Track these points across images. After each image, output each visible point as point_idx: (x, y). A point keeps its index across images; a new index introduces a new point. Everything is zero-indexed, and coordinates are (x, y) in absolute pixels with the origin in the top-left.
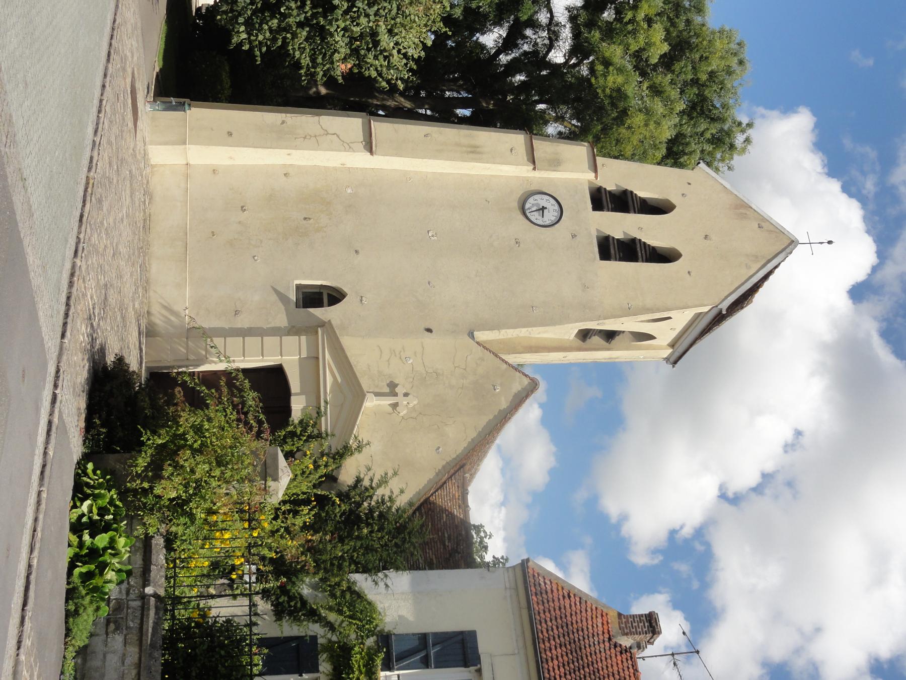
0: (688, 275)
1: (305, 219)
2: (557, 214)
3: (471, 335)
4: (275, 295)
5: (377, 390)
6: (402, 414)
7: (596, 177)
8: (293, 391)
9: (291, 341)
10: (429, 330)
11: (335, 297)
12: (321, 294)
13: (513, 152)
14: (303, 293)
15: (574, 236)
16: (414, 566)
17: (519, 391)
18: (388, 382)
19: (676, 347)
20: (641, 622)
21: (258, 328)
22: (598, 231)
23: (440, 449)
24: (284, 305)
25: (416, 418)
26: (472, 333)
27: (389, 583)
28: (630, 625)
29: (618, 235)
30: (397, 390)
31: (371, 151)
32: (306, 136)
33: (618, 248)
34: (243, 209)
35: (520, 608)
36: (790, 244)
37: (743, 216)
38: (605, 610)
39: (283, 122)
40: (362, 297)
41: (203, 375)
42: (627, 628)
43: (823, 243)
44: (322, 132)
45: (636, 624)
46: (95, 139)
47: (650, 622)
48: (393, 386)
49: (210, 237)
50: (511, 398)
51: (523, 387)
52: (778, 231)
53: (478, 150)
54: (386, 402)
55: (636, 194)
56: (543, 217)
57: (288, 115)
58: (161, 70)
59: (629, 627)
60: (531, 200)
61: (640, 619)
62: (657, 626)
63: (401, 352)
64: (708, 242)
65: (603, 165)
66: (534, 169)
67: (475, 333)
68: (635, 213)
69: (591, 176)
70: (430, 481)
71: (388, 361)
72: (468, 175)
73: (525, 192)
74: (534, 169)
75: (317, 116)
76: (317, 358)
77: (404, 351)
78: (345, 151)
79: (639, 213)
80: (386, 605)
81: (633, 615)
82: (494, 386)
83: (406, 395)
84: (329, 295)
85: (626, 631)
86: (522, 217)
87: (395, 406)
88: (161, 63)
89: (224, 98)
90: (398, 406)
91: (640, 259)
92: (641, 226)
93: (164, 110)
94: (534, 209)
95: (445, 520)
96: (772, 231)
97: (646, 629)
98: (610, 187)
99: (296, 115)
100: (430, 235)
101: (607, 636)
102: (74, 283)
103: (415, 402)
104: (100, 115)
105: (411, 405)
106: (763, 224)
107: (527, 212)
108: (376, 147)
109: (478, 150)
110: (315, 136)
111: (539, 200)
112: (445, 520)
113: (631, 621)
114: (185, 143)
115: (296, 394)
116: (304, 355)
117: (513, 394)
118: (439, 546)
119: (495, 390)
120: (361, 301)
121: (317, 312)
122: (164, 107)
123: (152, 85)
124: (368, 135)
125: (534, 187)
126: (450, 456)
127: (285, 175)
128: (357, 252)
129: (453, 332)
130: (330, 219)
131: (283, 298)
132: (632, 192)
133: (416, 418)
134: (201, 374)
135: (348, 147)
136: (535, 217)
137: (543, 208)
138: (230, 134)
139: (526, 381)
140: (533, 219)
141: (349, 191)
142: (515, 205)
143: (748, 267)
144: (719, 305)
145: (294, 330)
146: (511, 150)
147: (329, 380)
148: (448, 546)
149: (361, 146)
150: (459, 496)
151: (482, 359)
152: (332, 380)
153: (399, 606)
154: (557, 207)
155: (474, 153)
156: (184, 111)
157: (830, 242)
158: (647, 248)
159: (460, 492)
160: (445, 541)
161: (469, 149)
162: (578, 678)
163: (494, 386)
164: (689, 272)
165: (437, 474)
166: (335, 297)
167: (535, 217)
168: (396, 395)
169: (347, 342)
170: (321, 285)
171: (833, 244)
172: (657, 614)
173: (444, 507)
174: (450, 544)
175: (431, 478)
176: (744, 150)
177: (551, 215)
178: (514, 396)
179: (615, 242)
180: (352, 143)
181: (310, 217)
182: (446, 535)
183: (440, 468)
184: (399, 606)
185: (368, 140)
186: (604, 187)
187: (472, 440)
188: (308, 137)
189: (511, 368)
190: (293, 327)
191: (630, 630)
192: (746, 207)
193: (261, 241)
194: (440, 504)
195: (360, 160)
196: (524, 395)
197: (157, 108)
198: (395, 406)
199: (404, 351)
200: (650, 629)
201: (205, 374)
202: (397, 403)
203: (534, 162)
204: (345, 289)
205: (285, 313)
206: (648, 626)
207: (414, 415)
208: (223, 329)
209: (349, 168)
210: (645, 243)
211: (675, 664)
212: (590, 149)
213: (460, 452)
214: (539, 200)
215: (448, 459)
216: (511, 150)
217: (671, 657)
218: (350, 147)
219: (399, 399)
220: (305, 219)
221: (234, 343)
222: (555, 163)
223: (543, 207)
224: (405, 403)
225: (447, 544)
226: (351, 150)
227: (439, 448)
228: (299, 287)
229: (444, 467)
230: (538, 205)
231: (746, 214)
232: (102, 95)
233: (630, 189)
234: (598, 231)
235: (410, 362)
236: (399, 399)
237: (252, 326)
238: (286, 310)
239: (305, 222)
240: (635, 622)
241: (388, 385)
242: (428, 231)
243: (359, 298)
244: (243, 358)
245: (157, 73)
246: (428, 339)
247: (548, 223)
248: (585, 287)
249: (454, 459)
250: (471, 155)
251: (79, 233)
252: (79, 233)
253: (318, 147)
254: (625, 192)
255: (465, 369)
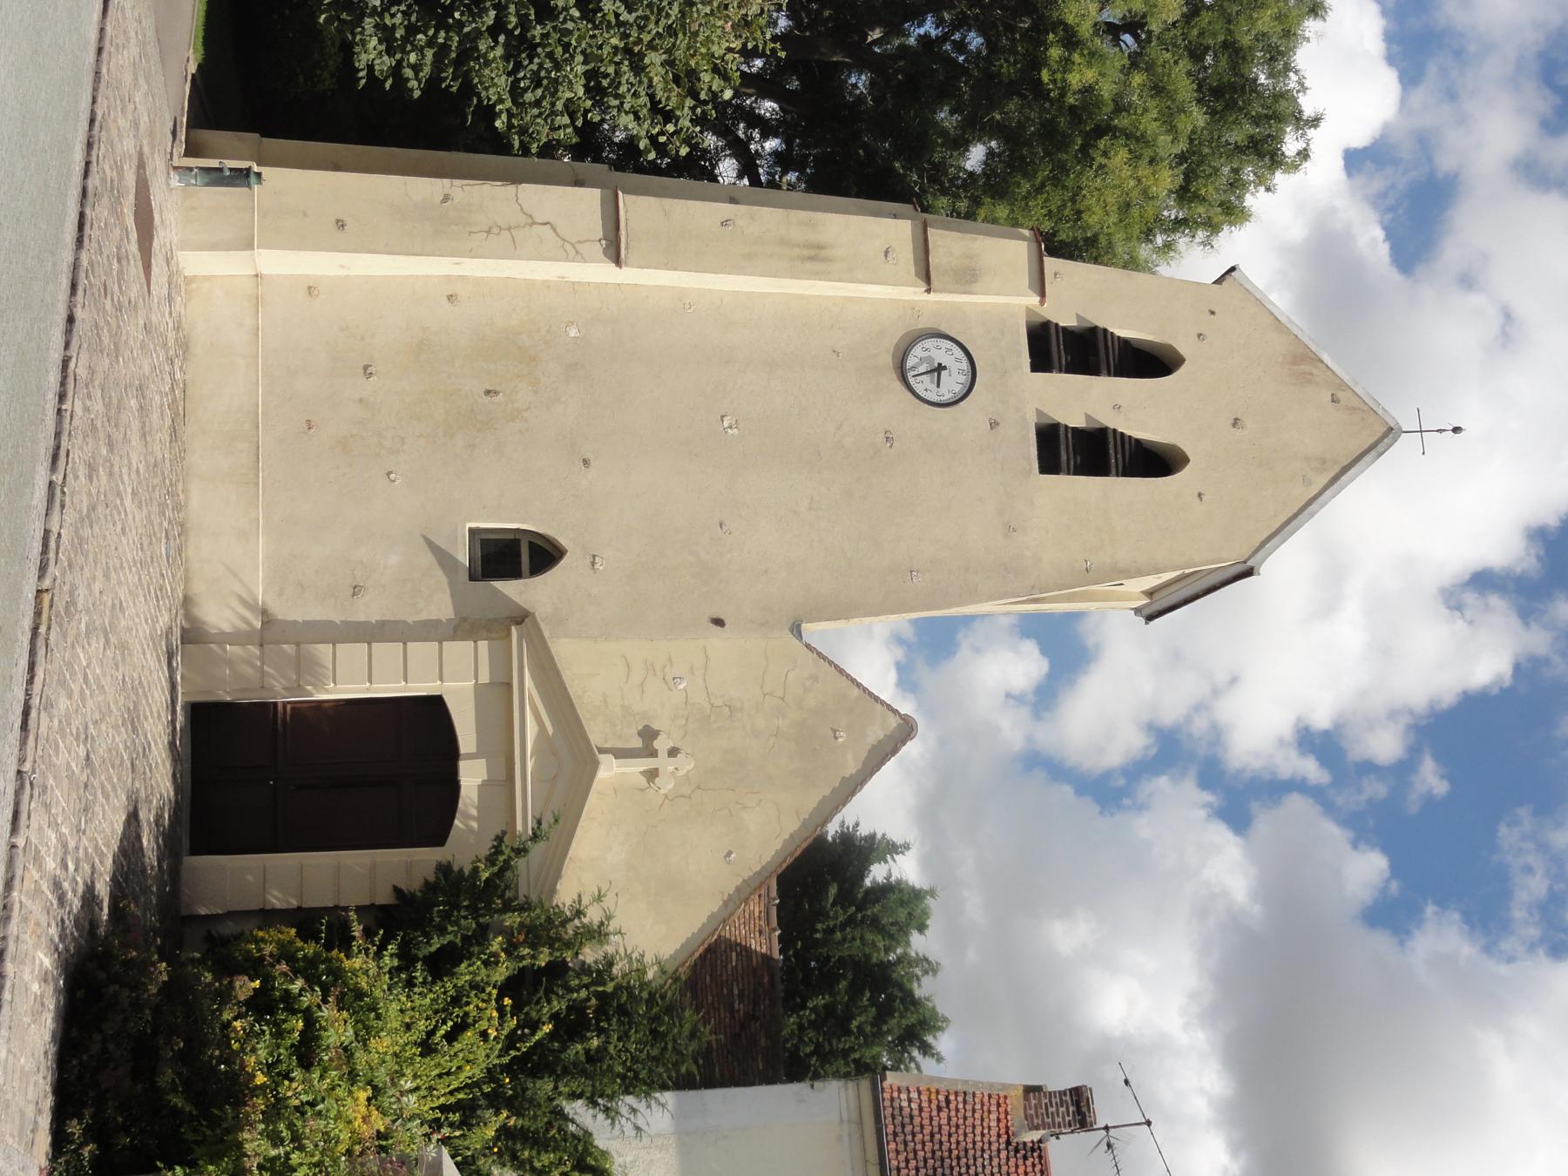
0: (1197, 500)
1: (488, 392)
2: (964, 379)
3: (796, 630)
4: (430, 554)
5: (620, 745)
6: (662, 791)
7: (1042, 303)
8: (463, 749)
9: (460, 651)
10: (719, 622)
11: (544, 555)
12: (516, 543)
13: (890, 256)
14: (483, 542)
15: (994, 425)
16: (684, 1083)
17: (879, 742)
18: (640, 728)
19: (1156, 597)
20: (1062, 1106)
21: (396, 622)
22: (1039, 413)
23: (733, 855)
24: (448, 577)
25: (689, 797)
26: (799, 626)
27: (640, 1122)
28: (1044, 1111)
29: (1074, 419)
30: (657, 744)
31: (617, 261)
32: (490, 228)
33: (1073, 444)
34: (367, 371)
35: (866, 1161)
36: (1385, 435)
37: (1305, 379)
38: (1002, 1094)
39: (446, 198)
40: (594, 556)
41: (292, 708)
42: (1037, 1118)
43: (1444, 430)
44: (523, 219)
45: (1054, 1109)
46: (54, 478)
47: (1077, 1104)
48: (649, 734)
49: (304, 433)
50: (865, 754)
51: (888, 733)
52: (1366, 408)
53: (823, 253)
54: (636, 767)
55: (1112, 333)
56: (938, 386)
57: (457, 182)
58: (200, 67)
59: (1042, 1114)
60: (917, 351)
61: (1061, 1099)
62: (1090, 1112)
63: (665, 667)
64: (1238, 432)
65: (1056, 274)
66: (928, 291)
67: (804, 626)
68: (1109, 375)
69: (1034, 300)
70: (712, 917)
71: (642, 685)
72: (801, 297)
73: (905, 335)
74: (928, 291)
75: (514, 182)
76: (509, 685)
77: (671, 665)
78: (567, 259)
79: (1116, 375)
80: (629, 1159)
81: (1050, 1093)
82: (835, 731)
83: (673, 752)
84: (531, 545)
85: (1036, 1121)
86: (898, 386)
87: (652, 775)
88: (200, 55)
89: (328, 76)
90: (657, 776)
91: (1114, 472)
92: (1120, 402)
93: (207, 185)
94: (923, 369)
95: (734, 964)
96: (1354, 409)
97: (1071, 1118)
98: (1067, 320)
99: (471, 182)
100: (726, 424)
101: (1004, 1137)
102: (11, 910)
103: (690, 767)
104: (64, 407)
105: (682, 773)
106: (1340, 395)
107: (910, 374)
108: (627, 248)
109: (823, 253)
110: (509, 229)
111: (933, 350)
112: (734, 964)
113: (1046, 1104)
114: (249, 246)
115: (470, 756)
116: (485, 678)
117: (869, 747)
118: (722, 1016)
119: (836, 738)
120: (593, 564)
121: (509, 589)
122: (207, 180)
123: (183, 116)
124: (611, 225)
125: (924, 324)
126: (750, 868)
127: (450, 297)
128: (586, 462)
129: (762, 625)
130: (535, 392)
131: (444, 559)
132: (1105, 331)
133: (689, 797)
134: (289, 707)
135: (573, 251)
136: (923, 385)
137: (940, 368)
138: (341, 224)
139: (893, 722)
140: (919, 389)
141: (573, 333)
142: (887, 360)
143: (1307, 482)
144: (1249, 559)
145: (464, 628)
146: (886, 253)
147: (531, 726)
148: (738, 1011)
149: (598, 249)
150: (760, 912)
151: (815, 678)
152: (536, 728)
153: (652, 1161)
154: (965, 365)
155: (815, 258)
156: (249, 186)
157: (1456, 430)
158: (1127, 446)
159: (762, 904)
160: (733, 1003)
161: (806, 252)
162: (947, 1172)
163: (835, 731)
164: (1200, 495)
165: (726, 904)
166: (544, 555)
167: (923, 385)
168: (653, 754)
169: (567, 652)
170: (518, 529)
171: (1463, 433)
172: (1091, 1089)
173: (733, 939)
174: (742, 1006)
175: (715, 911)
176: (1294, 167)
177: (953, 383)
178: (869, 751)
179: (1070, 431)
180: (579, 242)
181: (498, 389)
182: (736, 991)
183: (731, 892)
184: (652, 1161)
185: (612, 236)
186: (1055, 321)
187: (791, 835)
188: (495, 230)
189: (868, 697)
190: (464, 620)
191: (1043, 1120)
192: (1313, 359)
193: (403, 440)
194: (728, 935)
195: (601, 272)
196: (888, 749)
197: (193, 181)
198: (652, 775)
199: (671, 665)
200: (1078, 1118)
201: (298, 705)
202: (657, 769)
203: (927, 279)
204: (563, 541)
205: (448, 591)
206: (1073, 1112)
207: (686, 790)
208: (329, 624)
209: (573, 283)
210: (1122, 434)
211: (1109, 1146)
212: (1034, 245)
213: (769, 859)
214: (933, 350)
215: (747, 874)
216: (886, 253)
217: (1104, 1132)
218: (577, 252)
219: (662, 762)
220: (488, 392)
221: (351, 653)
222: (967, 277)
223: (940, 364)
224: (671, 768)
225: (736, 1006)
226: (578, 257)
227: (729, 854)
228: (473, 532)
229: (738, 889)
230: (930, 359)
231: (1311, 374)
232: (67, 346)
233: (1101, 324)
234: (1039, 413)
235: (681, 687)
236: (662, 762)
237: (384, 619)
238: (452, 585)
239: (487, 399)
240: (1052, 1106)
241: (640, 734)
242: (722, 417)
243: (589, 560)
244: (368, 684)
245: (193, 75)
246: (718, 641)
247: (947, 397)
248: (1010, 529)
249: (759, 873)
250: (809, 265)
251: (22, 760)
252: (22, 760)
253: (513, 251)
254: (1094, 330)
255: (783, 699)
